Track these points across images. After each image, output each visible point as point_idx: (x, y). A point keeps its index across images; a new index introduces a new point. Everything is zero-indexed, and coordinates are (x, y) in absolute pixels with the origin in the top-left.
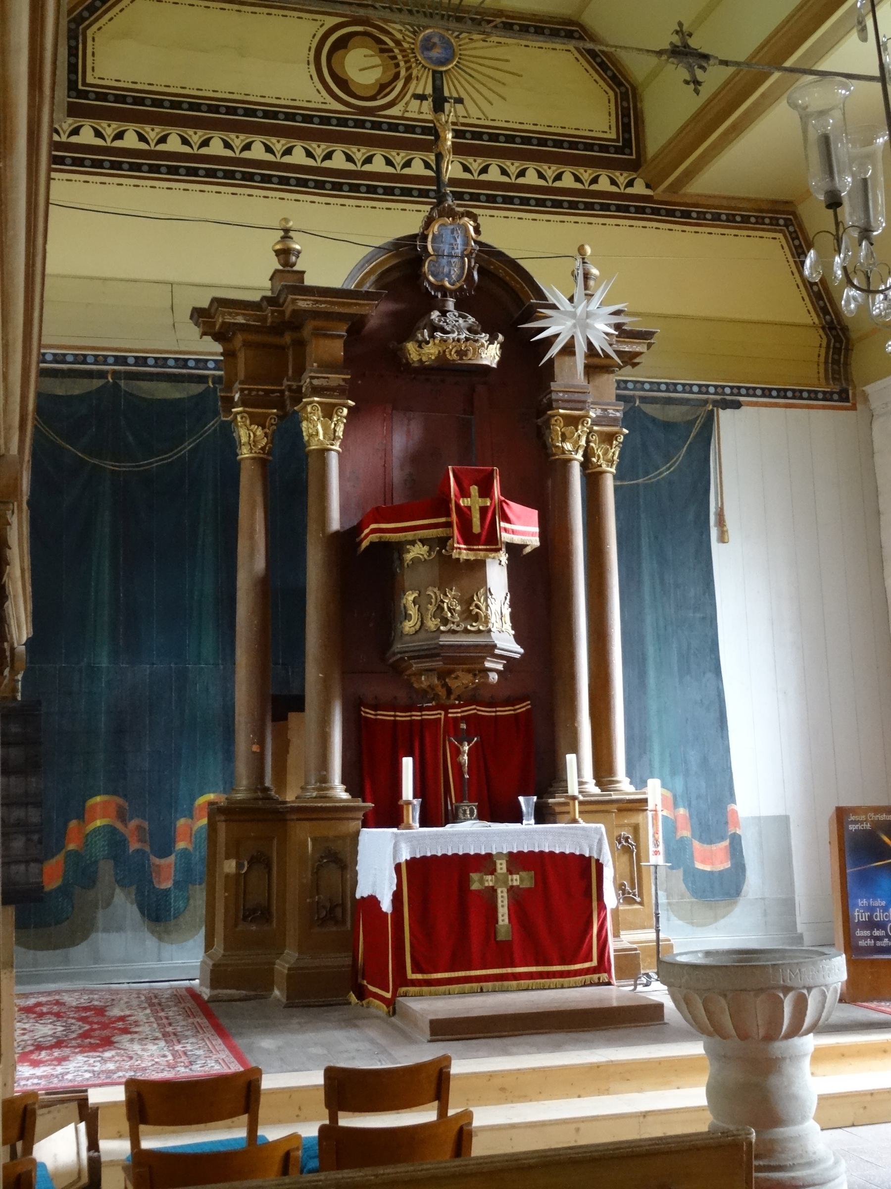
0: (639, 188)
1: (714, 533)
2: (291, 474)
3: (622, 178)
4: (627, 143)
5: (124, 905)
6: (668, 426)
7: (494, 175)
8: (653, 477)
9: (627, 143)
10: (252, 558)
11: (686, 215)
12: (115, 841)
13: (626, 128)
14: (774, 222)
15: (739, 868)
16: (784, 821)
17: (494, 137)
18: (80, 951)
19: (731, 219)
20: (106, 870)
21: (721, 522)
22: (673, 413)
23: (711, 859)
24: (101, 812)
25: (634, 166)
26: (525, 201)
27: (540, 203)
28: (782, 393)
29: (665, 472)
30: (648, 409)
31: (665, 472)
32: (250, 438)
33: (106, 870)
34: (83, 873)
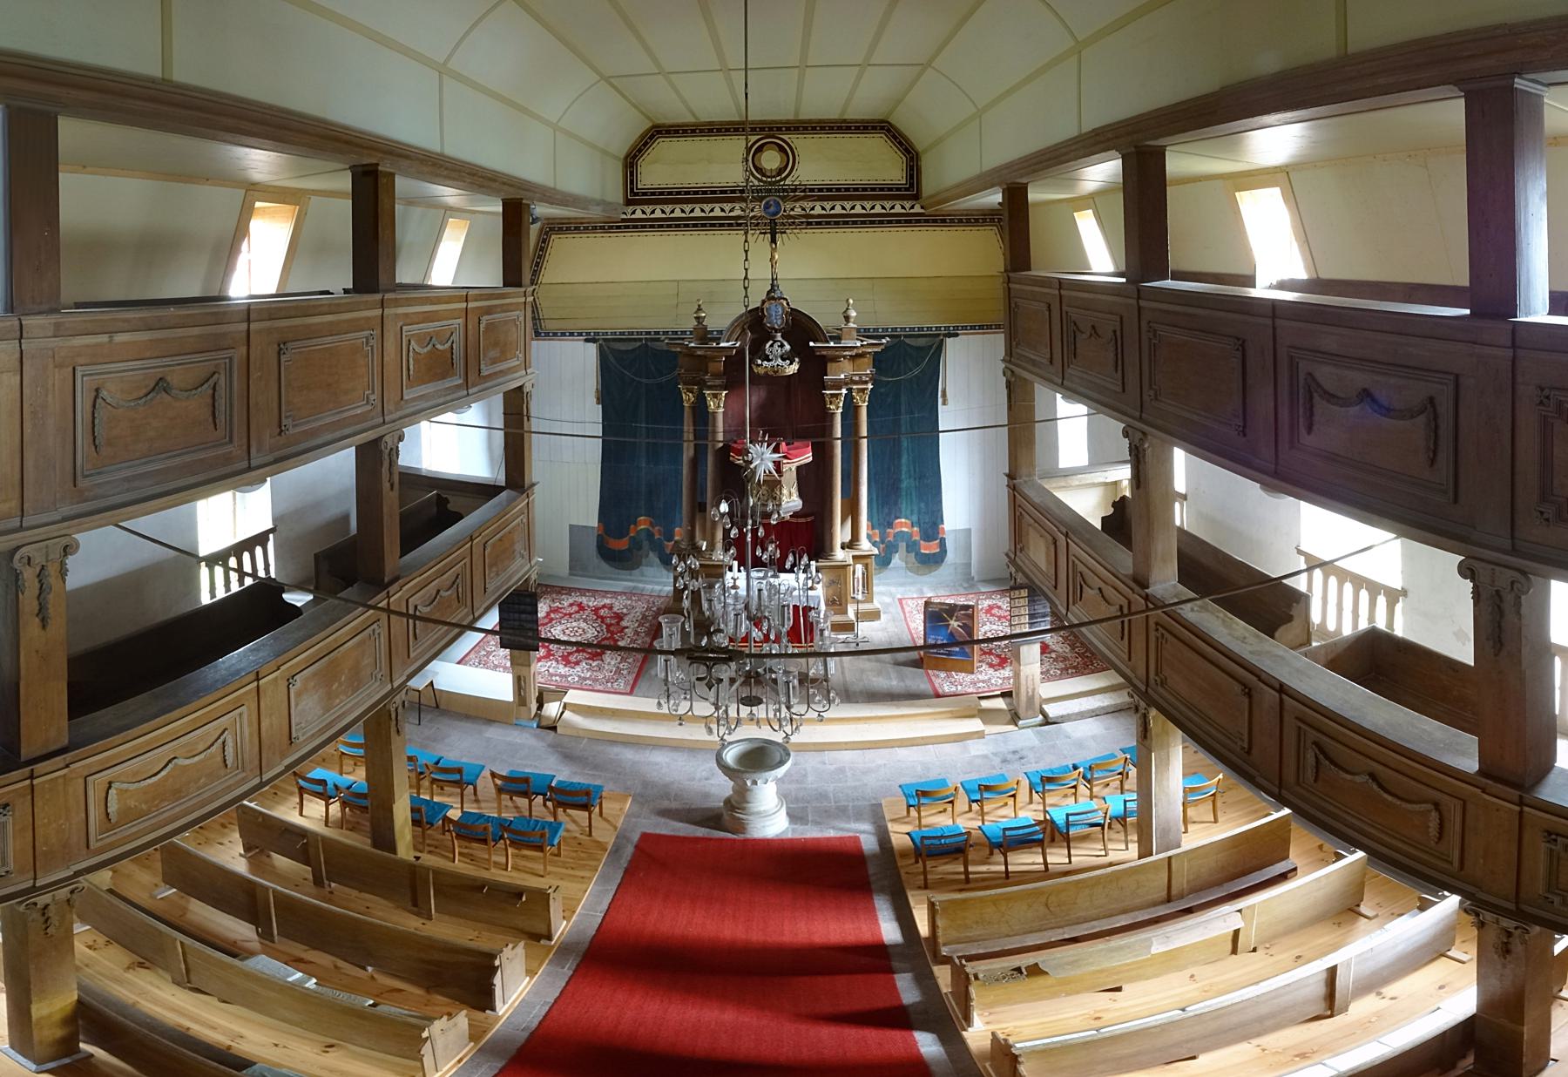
0: (918, 209)
1: (940, 400)
2: (702, 415)
3: (908, 205)
4: (912, 185)
5: (653, 557)
6: (919, 349)
7: (838, 210)
8: (909, 375)
9: (912, 185)
10: (688, 452)
11: (944, 221)
12: (650, 535)
13: (912, 177)
14: (992, 220)
15: (943, 551)
16: (969, 530)
17: (838, 190)
18: (636, 572)
19: (968, 221)
20: (646, 544)
21: (944, 395)
22: (921, 342)
23: (929, 548)
24: (643, 523)
25: (916, 197)
26: (855, 223)
27: (863, 222)
28: (981, 327)
29: (916, 372)
30: (907, 341)
31: (916, 372)
32: (688, 398)
33: (646, 544)
34: (636, 545)
